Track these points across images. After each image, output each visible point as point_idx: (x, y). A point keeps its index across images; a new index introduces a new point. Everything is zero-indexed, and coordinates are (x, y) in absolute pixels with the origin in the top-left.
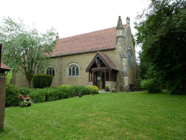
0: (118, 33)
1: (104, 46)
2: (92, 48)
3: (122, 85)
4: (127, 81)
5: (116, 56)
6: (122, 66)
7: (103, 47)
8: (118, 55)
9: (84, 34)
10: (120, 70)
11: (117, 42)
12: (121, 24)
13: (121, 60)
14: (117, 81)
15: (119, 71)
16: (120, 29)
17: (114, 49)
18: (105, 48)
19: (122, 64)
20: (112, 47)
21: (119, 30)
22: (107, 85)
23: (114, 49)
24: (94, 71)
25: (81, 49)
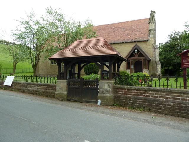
0: (151, 27)
1: (136, 38)
2: (124, 38)
3: (155, 72)
4: (160, 69)
5: (148, 47)
6: (156, 57)
7: (136, 39)
8: (151, 47)
9: (109, 24)
10: (152, 60)
11: (150, 35)
12: (153, 19)
13: (154, 51)
14: (150, 70)
15: (151, 61)
16: (153, 23)
17: (147, 41)
18: (137, 40)
19: (155, 54)
20: (145, 39)
21: (152, 23)
22: (145, 72)
23: (147, 41)
24: (131, 60)
25: (136, 37)
